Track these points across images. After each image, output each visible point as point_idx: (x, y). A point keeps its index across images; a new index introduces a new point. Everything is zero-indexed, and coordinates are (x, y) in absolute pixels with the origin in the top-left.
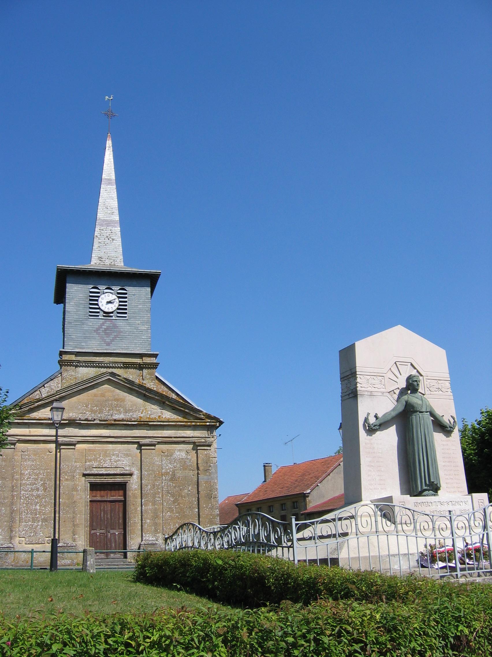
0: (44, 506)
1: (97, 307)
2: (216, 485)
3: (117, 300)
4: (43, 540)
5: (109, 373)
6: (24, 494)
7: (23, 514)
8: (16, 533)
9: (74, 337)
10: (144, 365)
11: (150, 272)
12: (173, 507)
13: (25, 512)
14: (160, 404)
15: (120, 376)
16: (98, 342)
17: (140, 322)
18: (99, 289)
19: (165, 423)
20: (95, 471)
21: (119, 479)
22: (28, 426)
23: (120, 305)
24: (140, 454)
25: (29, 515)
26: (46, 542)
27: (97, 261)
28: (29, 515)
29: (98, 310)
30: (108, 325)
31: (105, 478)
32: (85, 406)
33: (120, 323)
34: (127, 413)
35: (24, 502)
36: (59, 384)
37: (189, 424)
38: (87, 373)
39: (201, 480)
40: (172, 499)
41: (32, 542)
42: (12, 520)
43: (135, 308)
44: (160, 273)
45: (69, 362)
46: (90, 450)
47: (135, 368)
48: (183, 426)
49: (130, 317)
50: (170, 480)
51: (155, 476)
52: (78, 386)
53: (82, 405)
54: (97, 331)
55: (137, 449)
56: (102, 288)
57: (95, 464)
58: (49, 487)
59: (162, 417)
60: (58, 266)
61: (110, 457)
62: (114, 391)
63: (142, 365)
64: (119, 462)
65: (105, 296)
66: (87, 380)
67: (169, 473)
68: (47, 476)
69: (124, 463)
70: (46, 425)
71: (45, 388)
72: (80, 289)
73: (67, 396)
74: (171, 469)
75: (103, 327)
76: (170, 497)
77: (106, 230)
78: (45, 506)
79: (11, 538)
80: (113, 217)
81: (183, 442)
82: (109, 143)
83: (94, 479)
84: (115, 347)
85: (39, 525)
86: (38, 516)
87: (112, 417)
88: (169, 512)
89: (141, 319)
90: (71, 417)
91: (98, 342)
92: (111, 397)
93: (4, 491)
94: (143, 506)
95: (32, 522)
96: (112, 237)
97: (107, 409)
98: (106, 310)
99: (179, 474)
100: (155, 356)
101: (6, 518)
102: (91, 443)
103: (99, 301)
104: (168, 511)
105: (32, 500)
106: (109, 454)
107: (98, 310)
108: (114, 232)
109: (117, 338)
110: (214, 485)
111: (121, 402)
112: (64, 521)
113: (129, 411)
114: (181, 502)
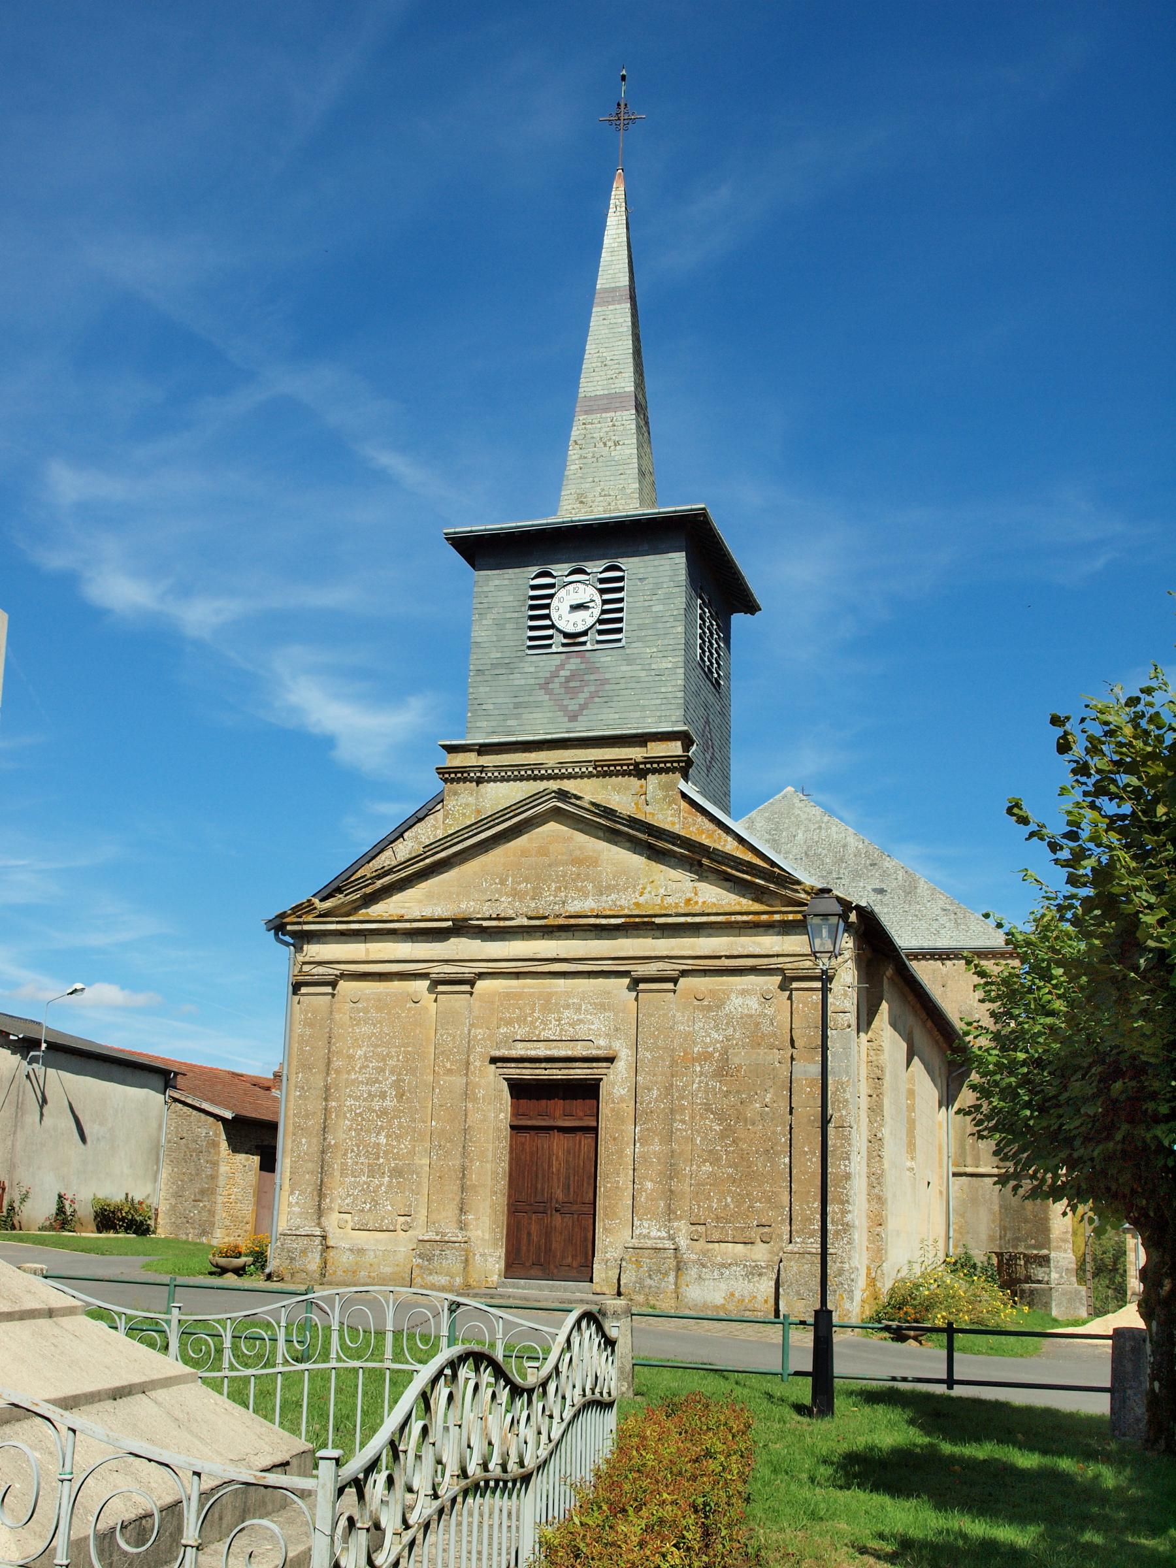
0: (397, 1137)
1: (547, 622)
2: (845, 1091)
3: (597, 598)
4: (392, 1223)
5: (554, 792)
7: (349, 1155)
8: (331, 1202)
9: (491, 707)
10: (648, 763)
11: (675, 512)
12: (719, 1148)
13: (352, 1151)
14: (692, 865)
15: (578, 798)
16: (549, 715)
17: (655, 650)
18: (554, 577)
19: (698, 919)
20: (519, 1051)
21: (579, 1072)
23: (604, 612)
25: (362, 1159)
26: (398, 1227)
27: (575, 506)
28: (362, 1159)
30: (574, 667)
31: (546, 1069)
32: (497, 881)
33: (605, 658)
34: (602, 894)
35: (352, 1125)
36: (436, 828)
37: (764, 917)
38: (618, 789)
39: (799, 1077)
40: (717, 1128)
42: (323, 1168)
43: (644, 615)
45: (605, 766)
46: (508, 995)
47: (624, 774)
48: (751, 925)
49: (629, 640)
50: (714, 1076)
51: (674, 1063)
52: (475, 831)
53: (492, 879)
54: (545, 686)
55: (629, 989)
56: (560, 570)
57: (521, 1033)
58: (409, 1091)
59: (697, 903)
60: (445, 531)
61: (559, 1012)
62: (570, 839)
63: (642, 763)
64: (582, 1026)
65: (568, 593)
66: (497, 815)
67: (711, 1055)
68: (407, 1062)
69: (593, 1027)
70: (404, 934)
71: (405, 843)
72: (506, 582)
74: (718, 1045)
76: (712, 1121)
77: (599, 422)
78: (398, 1138)
80: (619, 385)
81: (753, 970)
82: (617, 195)
83: (518, 1071)
84: (589, 724)
86: (381, 1160)
87: (563, 906)
88: (708, 1164)
89: (659, 642)
90: (463, 912)
91: (549, 715)
92: (563, 854)
93: (307, 1098)
94: (638, 1145)
95: (368, 1177)
97: (553, 885)
98: (570, 629)
99: (739, 1058)
102: (513, 976)
104: (705, 1161)
105: (369, 1121)
106: (556, 1004)
108: (619, 423)
109: (597, 700)
110: (837, 1089)
111: (588, 867)
112: (440, 1177)
113: (610, 889)
114: (743, 1136)
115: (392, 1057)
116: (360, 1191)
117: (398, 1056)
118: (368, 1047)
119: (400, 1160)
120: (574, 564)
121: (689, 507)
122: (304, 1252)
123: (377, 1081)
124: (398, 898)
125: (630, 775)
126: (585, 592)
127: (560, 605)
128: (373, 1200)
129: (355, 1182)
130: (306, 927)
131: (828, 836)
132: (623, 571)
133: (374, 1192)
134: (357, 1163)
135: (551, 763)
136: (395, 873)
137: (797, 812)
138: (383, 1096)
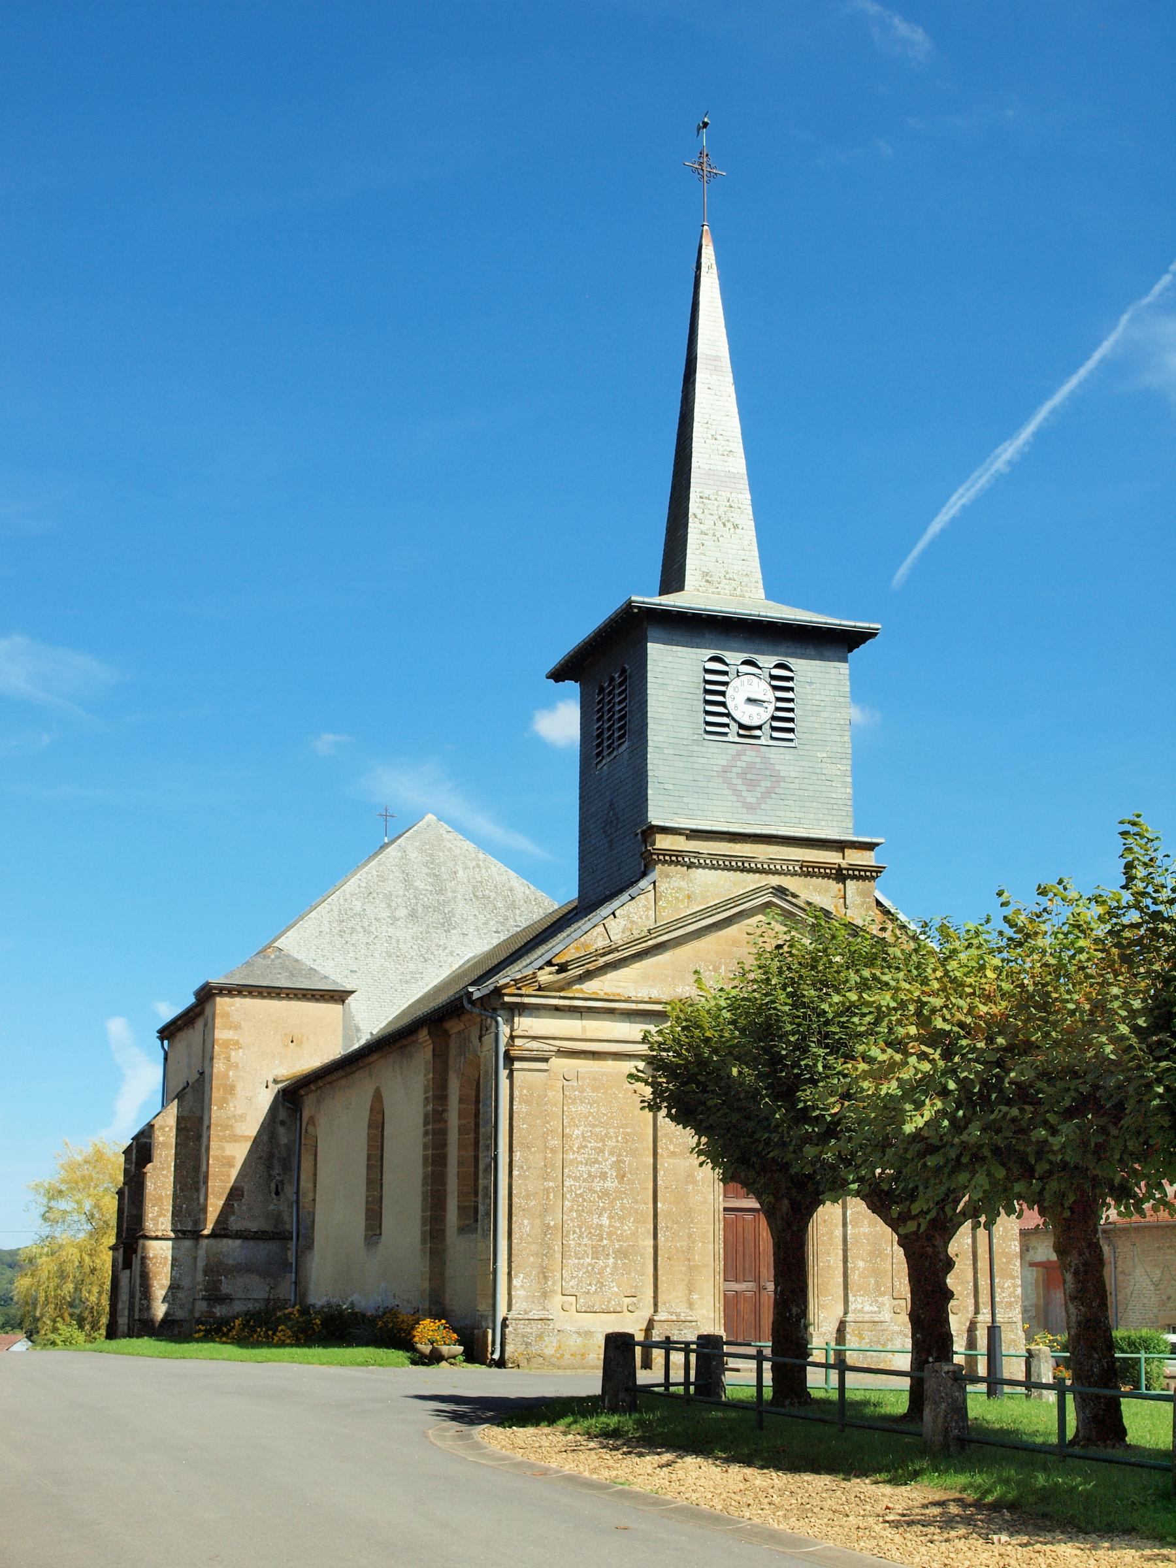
0: (619, 1219)
1: (721, 709)
5: (773, 888)
6: (571, 1186)
7: (571, 1237)
8: (553, 1285)
11: (855, 627)
13: (574, 1232)
15: (795, 896)
17: (825, 755)
22: (579, 1015)
24: (508, 1081)
25: (585, 1241)
29: (725, 720)
32: (711, 968)
35: (572, 1206)
36: (648, 909)
41: (593, 1307)
43: (813, 719)
44: (877, 629)
47: (826, 876)
63: (845, 869)
65: (742, 684)
68: (626, 1143)
70: (622, 1014)
73: (669, 943)
75: (739, 764)
78: (621, 1219)
79: (545, 1295)
85: (608, 1266)
86: (605, 1242)
93: (526, 1178)
94: (849, 1227)
95: (593, 1258)
96: (732, 520)
98: (745, 721)
100: (870, 847)
101: (534, 1246)
103: (727, 694)
107: (725, 720)
109: (773, 795)
112: (669, 1258)
115: (611, 1137)
116: (584, 1273)
117: (617, 1137)
118: (585, 1126)
119: (625, 1242)
120: (746, 655)
121: (866, 625)
122: (540, 1337)
123: (597, 1162)
124: (612, 975)
125: (829, 878)
126: (761, 689)
127: (735, 694)
128: (598, 1281)
129: (579, 1264)
130: (526, 1000)
131: (490, 876)
132: (791, 671)
133: (599, 1274)
134: (580, 1244)
135: (762, 858)
136: (618, 951)
137: (449, 845)
138: (604, 1176)
